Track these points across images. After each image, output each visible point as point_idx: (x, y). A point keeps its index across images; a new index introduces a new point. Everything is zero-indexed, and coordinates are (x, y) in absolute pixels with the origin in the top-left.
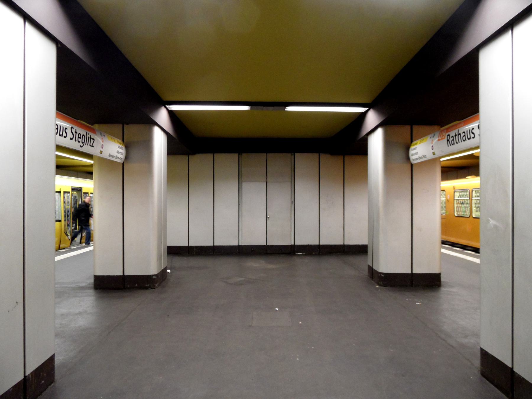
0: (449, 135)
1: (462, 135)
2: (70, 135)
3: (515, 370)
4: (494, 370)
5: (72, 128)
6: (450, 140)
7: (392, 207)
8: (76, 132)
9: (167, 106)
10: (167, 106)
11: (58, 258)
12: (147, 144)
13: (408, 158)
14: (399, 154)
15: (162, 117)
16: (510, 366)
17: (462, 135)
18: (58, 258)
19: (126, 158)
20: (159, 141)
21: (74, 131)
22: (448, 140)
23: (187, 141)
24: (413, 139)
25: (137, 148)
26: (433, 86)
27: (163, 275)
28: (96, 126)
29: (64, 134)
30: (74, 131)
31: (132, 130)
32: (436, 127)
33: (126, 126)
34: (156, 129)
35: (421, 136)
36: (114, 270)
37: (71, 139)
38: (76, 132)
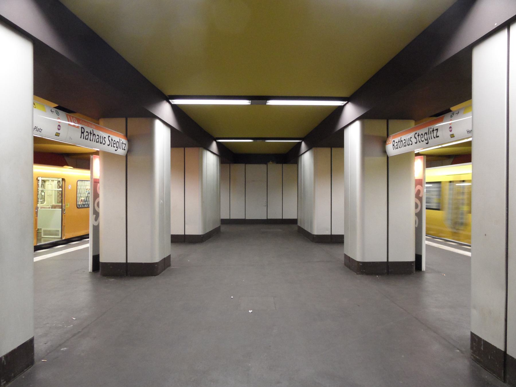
0: (394, 141)
1: (404, 142)
2: (108, 142)
3: (508, 353)
4: (482, 352)
5: (109, 136)
6: (395, 145)
7: (363, 194)
8: (112, 140)
9: (170, 101)
10: (170, 101)
11: (36, 259)
12: (149, 136)
13: (385, 152)
14: (377, 148)
15: (165, 111)
16: (502, 348)
17: (404, 142)
18: (36, 259)
19: (129, 151)
20: (162, 136)
21: (110, 139)
22: (393, 145)
23: (191, 134)
24: (390, 133)
25: (140, 140)
26: (418, 79)
27: (166, 262)
28: (102, 121)
29: (104, 142)
30: (110, 139)
31: (133, 122)
32: (412, 123)
33: (129, 119)
34: (157, 123)
35: (398, 131)
36: (180, 232)
37: (108, 145)
38: (112, 140)
